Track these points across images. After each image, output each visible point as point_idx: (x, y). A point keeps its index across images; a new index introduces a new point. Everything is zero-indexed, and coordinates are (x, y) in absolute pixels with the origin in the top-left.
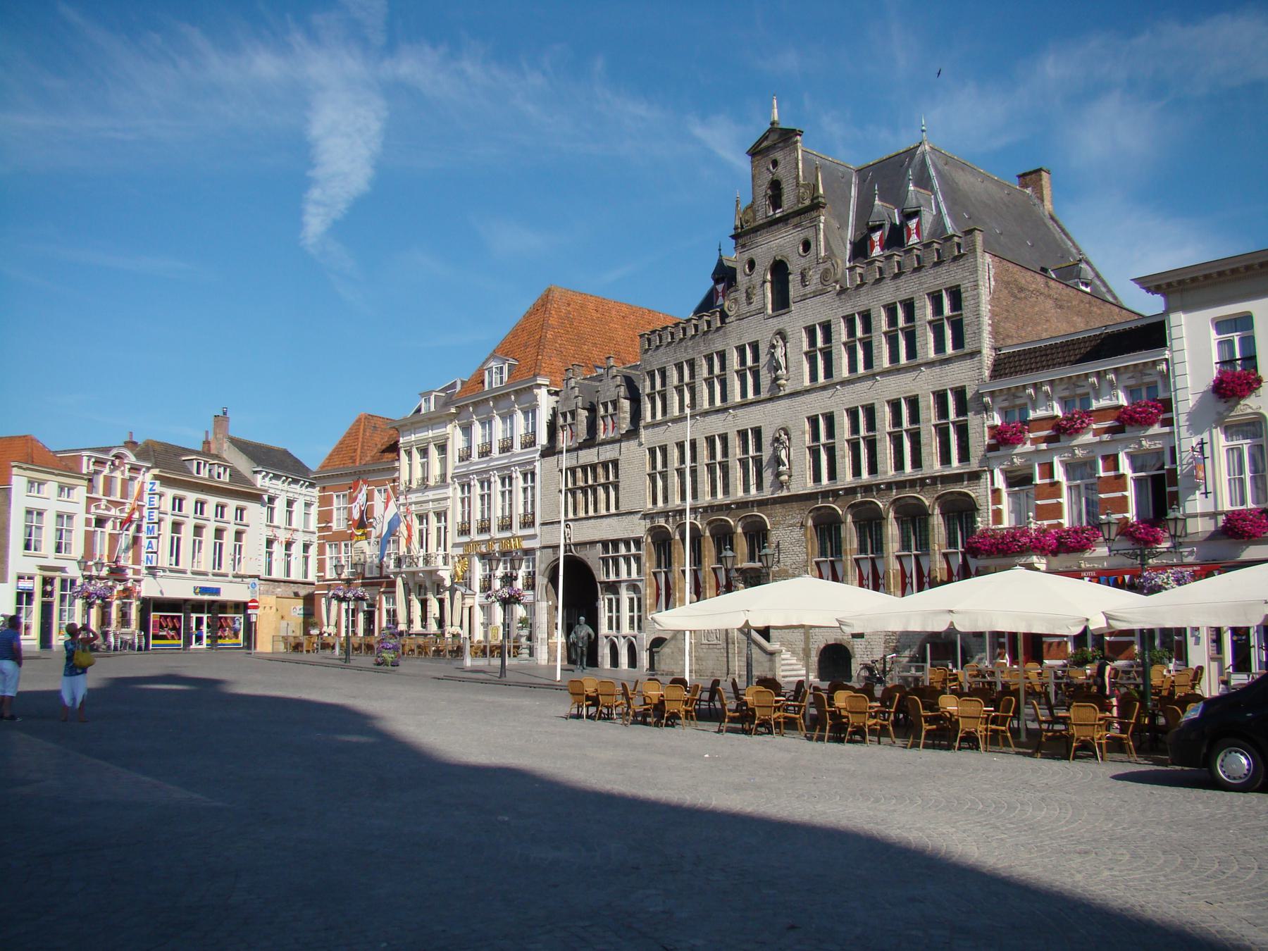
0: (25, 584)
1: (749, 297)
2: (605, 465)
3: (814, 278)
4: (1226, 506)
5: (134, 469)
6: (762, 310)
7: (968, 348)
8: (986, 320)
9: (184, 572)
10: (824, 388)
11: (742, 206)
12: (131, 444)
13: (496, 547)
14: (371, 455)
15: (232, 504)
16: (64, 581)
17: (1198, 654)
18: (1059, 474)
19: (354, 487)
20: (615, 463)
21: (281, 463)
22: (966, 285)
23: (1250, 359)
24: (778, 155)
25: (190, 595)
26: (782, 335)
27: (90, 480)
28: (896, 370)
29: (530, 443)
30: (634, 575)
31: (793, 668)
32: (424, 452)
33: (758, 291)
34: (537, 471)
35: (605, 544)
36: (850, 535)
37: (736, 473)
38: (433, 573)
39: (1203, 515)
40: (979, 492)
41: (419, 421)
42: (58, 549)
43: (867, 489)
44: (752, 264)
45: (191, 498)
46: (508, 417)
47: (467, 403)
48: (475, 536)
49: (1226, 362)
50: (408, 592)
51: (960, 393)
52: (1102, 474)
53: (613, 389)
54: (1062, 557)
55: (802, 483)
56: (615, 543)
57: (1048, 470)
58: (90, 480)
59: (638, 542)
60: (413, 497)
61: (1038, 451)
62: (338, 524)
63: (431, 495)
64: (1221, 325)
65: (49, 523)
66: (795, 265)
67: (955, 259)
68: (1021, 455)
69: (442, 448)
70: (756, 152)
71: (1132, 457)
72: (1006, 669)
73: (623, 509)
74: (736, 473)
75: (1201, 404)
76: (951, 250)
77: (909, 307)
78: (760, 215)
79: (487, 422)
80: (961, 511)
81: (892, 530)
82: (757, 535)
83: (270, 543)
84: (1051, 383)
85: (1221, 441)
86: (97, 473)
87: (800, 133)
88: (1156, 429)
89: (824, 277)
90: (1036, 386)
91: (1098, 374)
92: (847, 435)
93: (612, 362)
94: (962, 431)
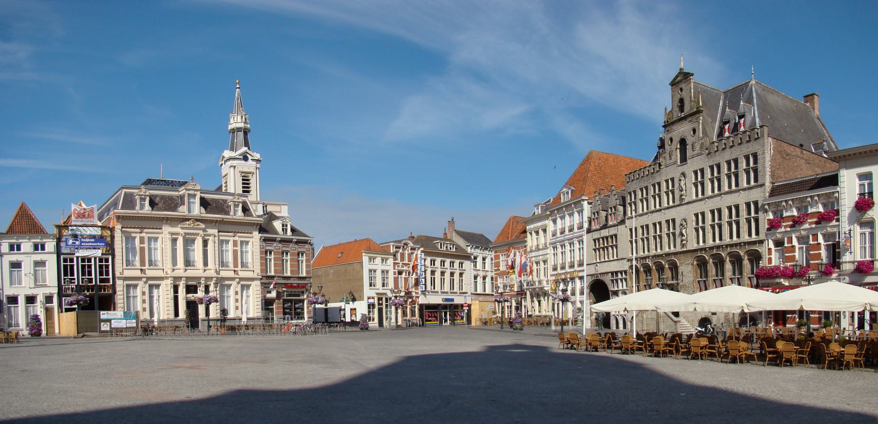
0: (371, 301)
1: (670, 156)
2: (611, 237)
3: (697, 147)
4: (859, 259)
5: (413, 249)
6: (675, 163)
7: (760, 182)
8: (768, 170)
9: (437, 292)
10: (701, 200)
11: (668, 111)
12: (412, 238)
13: (568, 276)
14: (515, 235)
15: (457, 262)
16: (386, 299)
17: (845, 323)
18: (795, 242)
19: (508, 250)
20: (616, 236)
21: (479, 241)
22: (759, 152)
23: (871, 194)
24: (683, 86)
25: (441, 302)
26: (683, 174)
27: (394, 256)
28: (730, 192)
29: (580, 227)
30: (625, 288)
31: (688, 327)
32: (537, 233)
33: (674, 153)
34: (585, 240)
35: (612, 273)
36: (712, 269)
37: (665, 239)
38: (542, 288)
39: (849, 262)
40: (763, 249)
41: (535, 219)
42: (383, 286)
43: (718, 247)
44: (671, 140)
45: (438, 260)
46: (571, 215)
47: (554, 209)
48: (559, 271)
49: (862, 194)
50: (532, 297)
51: (756, 203)
52: (811, 242)
53: (613, 201)
54: (794, 279)
55: (692, 245)
56: (616, 273)
57: (790, 240)
58: (394, 256)
59: (625, 272)
60: (533, 254)
61: (786, 232)
62: (503, 268)
63: (541, 253)
64: (861, 177)
65: (379, 275)
66: (689, 141)
67: (756, 139)
68: (780, 233)
69: (545, 231)
70: (673, 84)
71: (824, 235)
72: (772, 329)
73: (619, 257)
74: (665, 239)
75: (850, 215)
76: (753, 136)
77: (736, 161)
78: (675, 114)
79: (562, 218)
80: (756, 257)
81: (728, 266)
82: (674, 268)
83: (476, 277)
84: (792, 200)
85: (857, 229)
86: (397, 252)
87: (692, 75)
88: (834, 223)
89: (701, 148)
90: (786, 201)
91: (811, 197)
92: (710, 223)
93: (613, 188)
94: (757, 220)
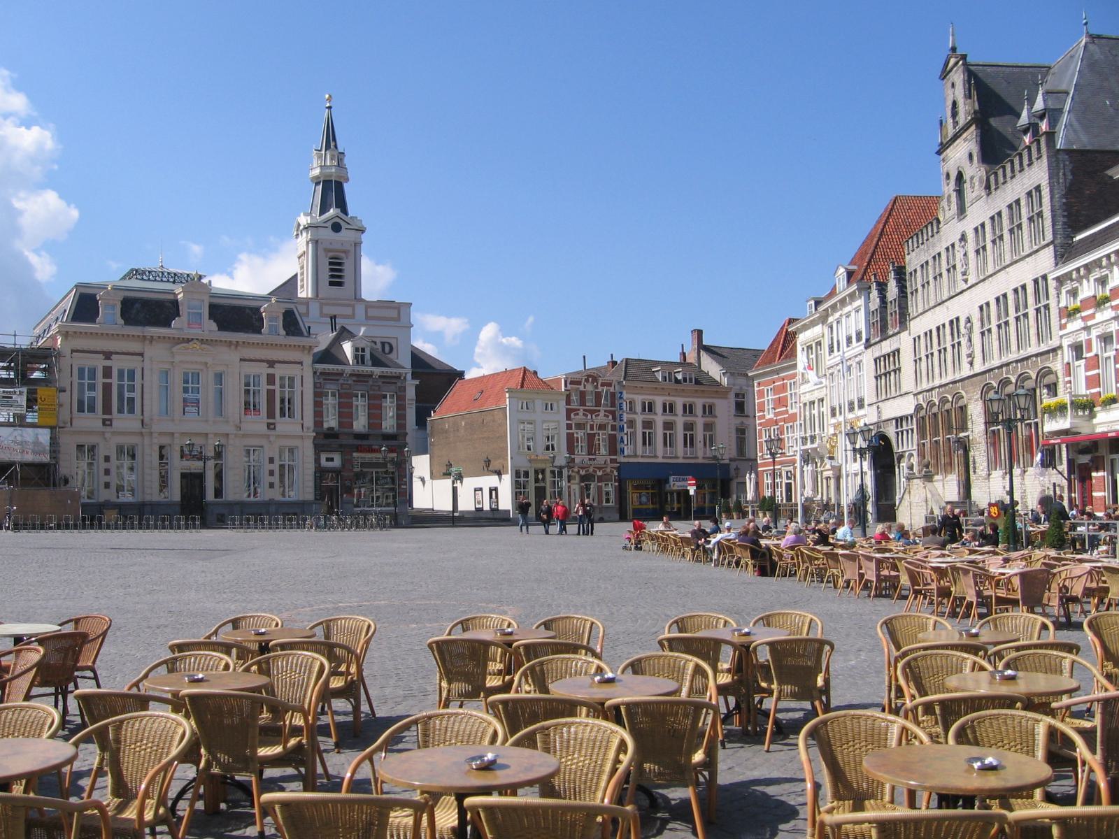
20: (898, 350)
